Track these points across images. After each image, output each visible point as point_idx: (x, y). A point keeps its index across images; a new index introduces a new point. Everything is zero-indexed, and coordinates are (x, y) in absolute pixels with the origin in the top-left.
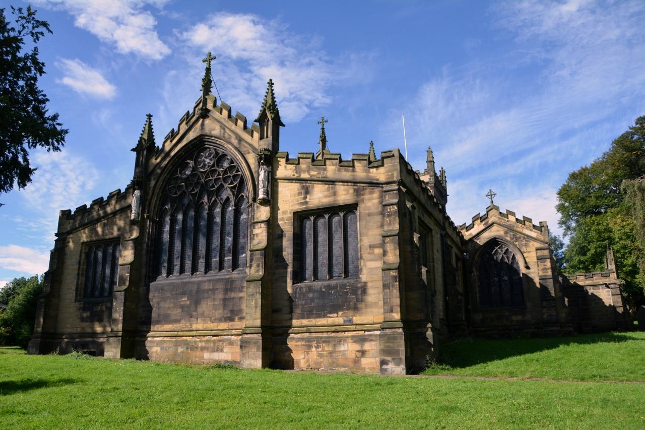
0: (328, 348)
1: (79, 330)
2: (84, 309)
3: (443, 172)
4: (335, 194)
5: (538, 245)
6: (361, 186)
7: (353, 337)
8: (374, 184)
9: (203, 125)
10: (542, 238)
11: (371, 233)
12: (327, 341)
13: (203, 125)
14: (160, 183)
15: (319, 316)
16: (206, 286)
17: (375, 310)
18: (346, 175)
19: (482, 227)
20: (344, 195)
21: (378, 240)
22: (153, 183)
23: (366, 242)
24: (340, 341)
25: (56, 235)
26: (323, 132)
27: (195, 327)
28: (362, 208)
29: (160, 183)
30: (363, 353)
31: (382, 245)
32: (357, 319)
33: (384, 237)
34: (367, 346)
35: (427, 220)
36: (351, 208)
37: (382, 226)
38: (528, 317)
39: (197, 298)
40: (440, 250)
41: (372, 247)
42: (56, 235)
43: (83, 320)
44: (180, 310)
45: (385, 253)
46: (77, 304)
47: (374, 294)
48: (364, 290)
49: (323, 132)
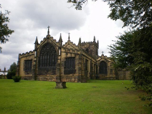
0: (70, 79)
1: (25, 76)
2: (25, 72)
3: (98, 41)
4: (72, 55)
5: (111, 63)
6: (76, 54)
7: (74, 78)
8: (78, 54)
9: (48, 40)
10: (111, 61)
11: (77, 62)
12: (70, 78)
13: (48, 40)
14: (40, 50)
15: (69, 74)
16: (49, 69)
17: (77, 74)
18: (74, 52)
19: (100, 59)
20: (73, 56)
21: (78, 63)
22: (38, 50)
23: (76, 63)
24: (72, 78)
25: (18, 58)
26: (69, 36)
27: (47, 76)
28: (76, 58)
29: (40, 50)
30: (75, 80)
31: (79, 64)
32: (74, 75)
33: (79, 63)
34: (76, 79)
35: (87, 59)
36: (74, 58)
37: (79, 61)
38: (108, 76)
39: (48, 71)
40: (90, 64)
41: (77, 64)
42: (18, 58)
43: (25, 74)
44: (45, 73)
45: (79, 65)
46: (24, 71)
47: (77, 71)
48: (76, 71)
49: (69, 36)
